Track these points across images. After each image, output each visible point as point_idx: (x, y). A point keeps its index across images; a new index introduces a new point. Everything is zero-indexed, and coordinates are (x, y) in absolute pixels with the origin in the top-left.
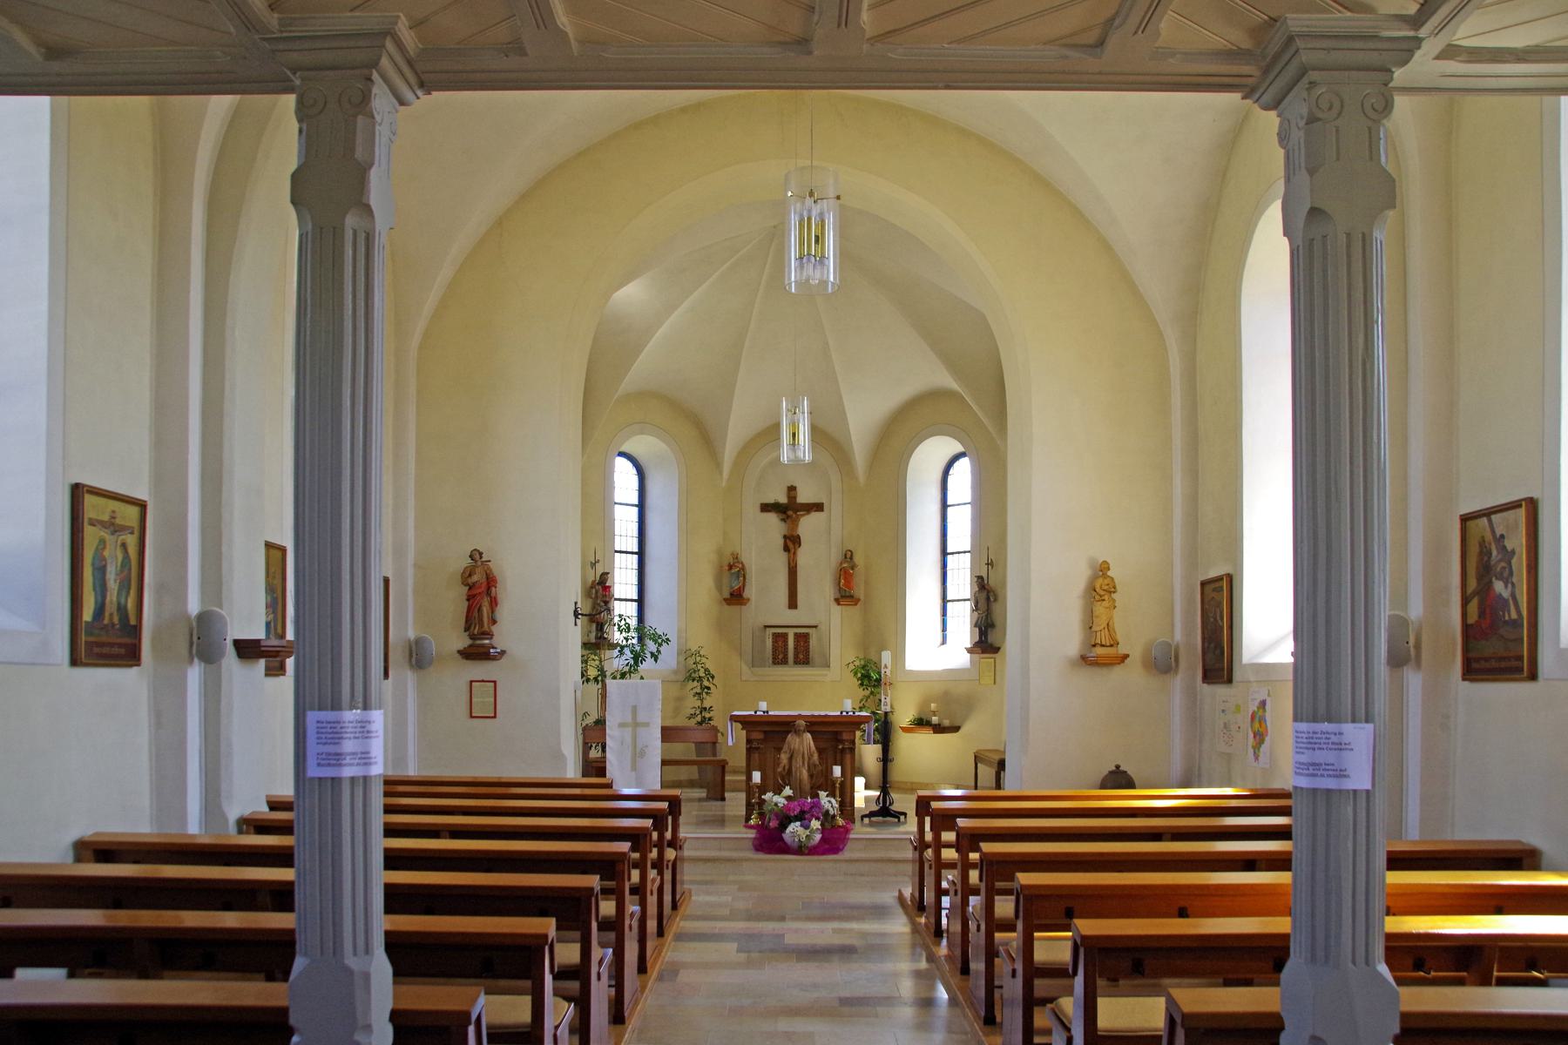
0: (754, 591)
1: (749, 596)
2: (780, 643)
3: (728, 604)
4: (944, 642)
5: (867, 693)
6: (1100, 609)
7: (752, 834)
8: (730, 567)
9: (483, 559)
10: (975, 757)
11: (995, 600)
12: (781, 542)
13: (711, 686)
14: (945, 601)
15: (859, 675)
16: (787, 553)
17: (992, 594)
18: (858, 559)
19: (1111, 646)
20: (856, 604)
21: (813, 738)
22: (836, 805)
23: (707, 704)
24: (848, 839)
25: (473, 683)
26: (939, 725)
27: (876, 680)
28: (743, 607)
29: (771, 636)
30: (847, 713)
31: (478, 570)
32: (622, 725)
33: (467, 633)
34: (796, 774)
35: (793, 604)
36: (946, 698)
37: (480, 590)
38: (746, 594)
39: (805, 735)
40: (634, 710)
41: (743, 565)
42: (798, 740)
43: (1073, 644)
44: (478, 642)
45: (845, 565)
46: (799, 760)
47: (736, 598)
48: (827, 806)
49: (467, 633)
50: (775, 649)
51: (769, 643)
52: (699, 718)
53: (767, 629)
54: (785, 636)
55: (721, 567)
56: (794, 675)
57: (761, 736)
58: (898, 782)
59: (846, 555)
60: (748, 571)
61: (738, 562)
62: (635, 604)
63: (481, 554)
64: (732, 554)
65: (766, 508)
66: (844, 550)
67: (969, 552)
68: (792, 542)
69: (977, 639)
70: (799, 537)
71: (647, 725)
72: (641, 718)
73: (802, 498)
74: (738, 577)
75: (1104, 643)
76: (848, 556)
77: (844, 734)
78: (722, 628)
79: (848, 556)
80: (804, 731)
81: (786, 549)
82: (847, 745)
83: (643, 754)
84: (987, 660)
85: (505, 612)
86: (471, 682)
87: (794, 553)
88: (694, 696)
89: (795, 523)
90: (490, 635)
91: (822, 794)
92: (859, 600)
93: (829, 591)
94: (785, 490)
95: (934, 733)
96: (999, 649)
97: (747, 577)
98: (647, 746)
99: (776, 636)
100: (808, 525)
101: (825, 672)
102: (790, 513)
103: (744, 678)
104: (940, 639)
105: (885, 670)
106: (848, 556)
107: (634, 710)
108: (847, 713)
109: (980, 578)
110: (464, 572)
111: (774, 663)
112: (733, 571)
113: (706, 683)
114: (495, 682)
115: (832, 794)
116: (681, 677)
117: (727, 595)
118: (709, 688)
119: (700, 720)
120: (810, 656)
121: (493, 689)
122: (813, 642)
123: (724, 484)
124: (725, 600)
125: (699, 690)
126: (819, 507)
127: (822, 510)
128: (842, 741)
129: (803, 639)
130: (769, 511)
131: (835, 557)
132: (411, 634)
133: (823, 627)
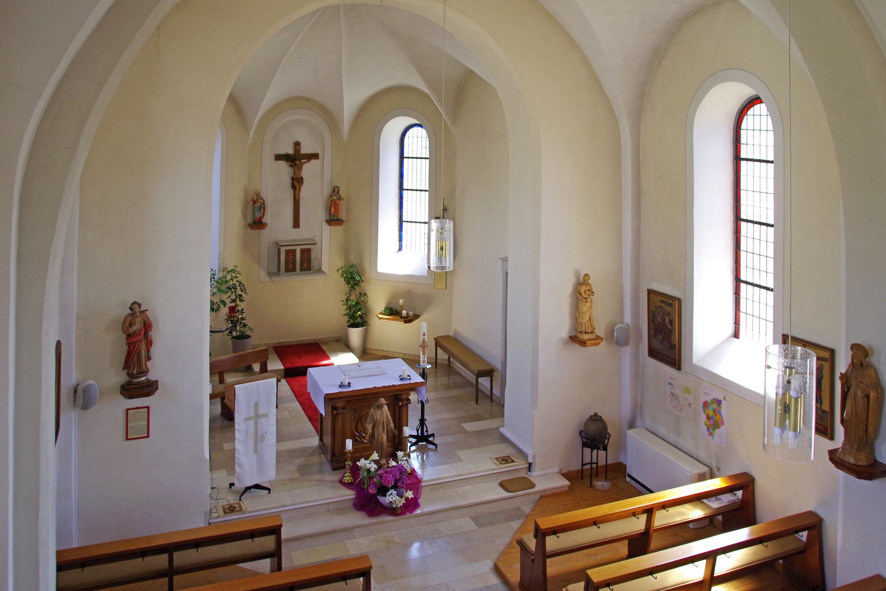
1: (266, 222)
2: (291, 257)
4: (400, 249)
7: (350, 494)
9: (141, 309)
16: (626, 556)
18: (342, 192)
25: (129, 411)
29: (284, 253)
33: (125, 371)
34: (378, 437)
35: (296, 224)
36: (409, 294)
37: (139, 338)
38: (264, 220)
41: (264, 201)
43: (565, 331)
44: (136, 380)
45: (334, 198)
47: (258, 224)
49: (125, 371)
54: (294, 251)
60: (266, 205)
61: (260, 198)
63: (140, 305)
65: (278, 157)
66: (333, 186)
68: (297, 182)
70: (302, 178)
72: (262, 411)
73: (304, 151)
75: (587, 331)
78: (246, 245)
79: (336, 190)
81: (294, 187)
83: (263, 438)
85: (156, 350)
86: (128, 410)
89: (300, 168)
93: (321, 214)
94: (293, 144)
97: (266, 208)
98: (266, 433)
99: (287, 252)
100: (308, 170)
103: (261, 280)
104: (397, 247)
105: (424, 337)
106: (335, 190)
107: (257, 405)
110: (124, 322)
112: (256, 205)
123: (249, 142)
126: (315, 156)
127: (318, 158)
129: (306, 253)
130: (282, 160)
131: (327, 191)
132: (74, 380)
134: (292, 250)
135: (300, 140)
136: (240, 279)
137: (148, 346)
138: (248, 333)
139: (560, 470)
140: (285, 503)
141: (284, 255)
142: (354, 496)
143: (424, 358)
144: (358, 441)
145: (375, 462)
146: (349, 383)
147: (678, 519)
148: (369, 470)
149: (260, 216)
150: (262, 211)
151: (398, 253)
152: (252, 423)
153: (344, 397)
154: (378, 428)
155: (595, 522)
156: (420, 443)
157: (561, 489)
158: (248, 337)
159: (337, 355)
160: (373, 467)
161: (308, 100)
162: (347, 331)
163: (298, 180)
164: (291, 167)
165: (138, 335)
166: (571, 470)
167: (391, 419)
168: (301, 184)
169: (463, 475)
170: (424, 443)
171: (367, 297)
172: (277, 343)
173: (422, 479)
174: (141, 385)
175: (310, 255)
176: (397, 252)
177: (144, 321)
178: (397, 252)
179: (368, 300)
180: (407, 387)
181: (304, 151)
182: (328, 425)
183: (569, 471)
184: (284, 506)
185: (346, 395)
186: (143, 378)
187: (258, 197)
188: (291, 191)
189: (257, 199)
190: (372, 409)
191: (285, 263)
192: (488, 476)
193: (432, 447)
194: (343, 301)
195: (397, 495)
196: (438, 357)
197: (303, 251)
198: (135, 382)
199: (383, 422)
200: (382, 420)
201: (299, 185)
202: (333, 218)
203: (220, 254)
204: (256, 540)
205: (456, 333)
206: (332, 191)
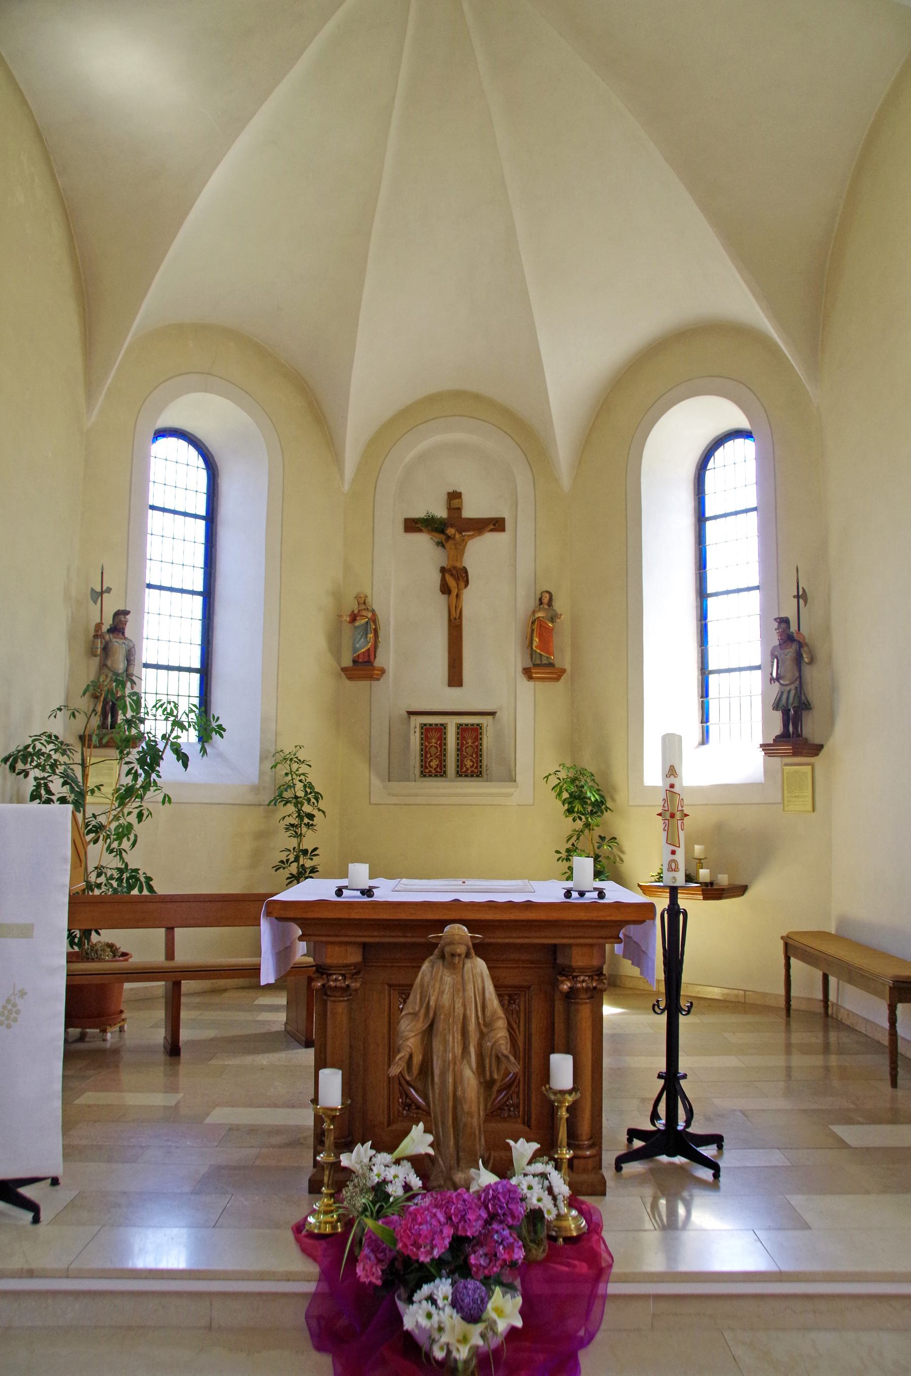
0: (392, 655)
2: (434, 741)
3: (350, 678)
5: (579, 824)
10: (786, 945)
11: (812, 661)
12: (435, 578)
13: (315, 812)
14: (704, 672)
15: (565, 795)
16: (445, 596)
17: (805, 649)
18: (559, 605)
20: (558, 679)
21: (489, 968)
22: (562, 1189)
23: (307, 844)
24: (605, 1297)
26: (712, 884)
27: (594, 804)
28: (375, 683)
29: (418, 730)
30: (582, 894)
34: (443, 1074)
35: (455, 678)
38: (378, 662)
39: (468, 964)
42: (448, 979)
48: (536, 1197)
50: (424, 753)
51: (415, 740)
52: (293, 869)
53: (413, 718)
54: (441, 729)
56: (465, 795)
57: (354, 957)
59: (540, 599)
62: (196, 677)
64: (357, 597)
65: (412, 525)
67: (757, 588)
69: (778, 729)
70: (465, 571)
73: (469, 512)
74: (366, 634)
76: (546, 600)
77: (575, 951)
79: (546, 600)
80: (468, 955)
81: (445, 589)
82: (583, 982)
84: (800, 768)
87: (457, 596)
88: (287, 829)
89: (460, 550)
91: (523, 1149)
95: (705, 898)
96: (821, 747)
97: (381, 634)
98: (23, 994)
99: (426, 730)
101: (511, 790)
102: (451, 531)
103: (373, 800)
106: (545, 601)
108: (582, 894)
109: (784, 622)
111: (423, 774)
112: (357, 624)
113: (307, 808)
115: (547, 1150)
116: (267, 797)
117: (347, 662)
118: (311, 816)
119: (295, 872)
120: (485, 763)
122: (488, 741)
123: (346, 487)
124: (344, 670)
125: (295, 821)
126: (498, 525)
127: (503, 530)
128: (567, 971)
130: (420, 531)
131: (524, 603)
133: (503, 715)
141: (418, 734)
142: (310, 1287)
143: (673, 852)
144: (418, 1107)
145: (419, 1163)
148: (380, 1190)
149: (366, 648)
150: (371, 636)
151: (698, 749)
154: (445, 1042)
156: (664, 1158)
160: (406, 1174)
161: (477, 397)
163: (454, 572)
164: (440, 549)
167: (500, 1013)
168: (462, 584)
169: (81, 1274)
170: (679, 1160)
171: (622, 852)
173: (610, 1266)
176: (697, 747)
178: (697, 747)
181: (469, 512)
182: (406, 1087)
184: (31, 1274)
187: (363, 607)
188: (441, 601)
189: (359, 611)
190: (426, 966)
193: (706, 1174)
194: (558, 852)
195: (454, 1304)
196: (792, 994)
197: (462, 730)
199: (465, 1018)
202: (538, 662)
203: (265, 720)
205: (843, 922)
206: (538, 602)
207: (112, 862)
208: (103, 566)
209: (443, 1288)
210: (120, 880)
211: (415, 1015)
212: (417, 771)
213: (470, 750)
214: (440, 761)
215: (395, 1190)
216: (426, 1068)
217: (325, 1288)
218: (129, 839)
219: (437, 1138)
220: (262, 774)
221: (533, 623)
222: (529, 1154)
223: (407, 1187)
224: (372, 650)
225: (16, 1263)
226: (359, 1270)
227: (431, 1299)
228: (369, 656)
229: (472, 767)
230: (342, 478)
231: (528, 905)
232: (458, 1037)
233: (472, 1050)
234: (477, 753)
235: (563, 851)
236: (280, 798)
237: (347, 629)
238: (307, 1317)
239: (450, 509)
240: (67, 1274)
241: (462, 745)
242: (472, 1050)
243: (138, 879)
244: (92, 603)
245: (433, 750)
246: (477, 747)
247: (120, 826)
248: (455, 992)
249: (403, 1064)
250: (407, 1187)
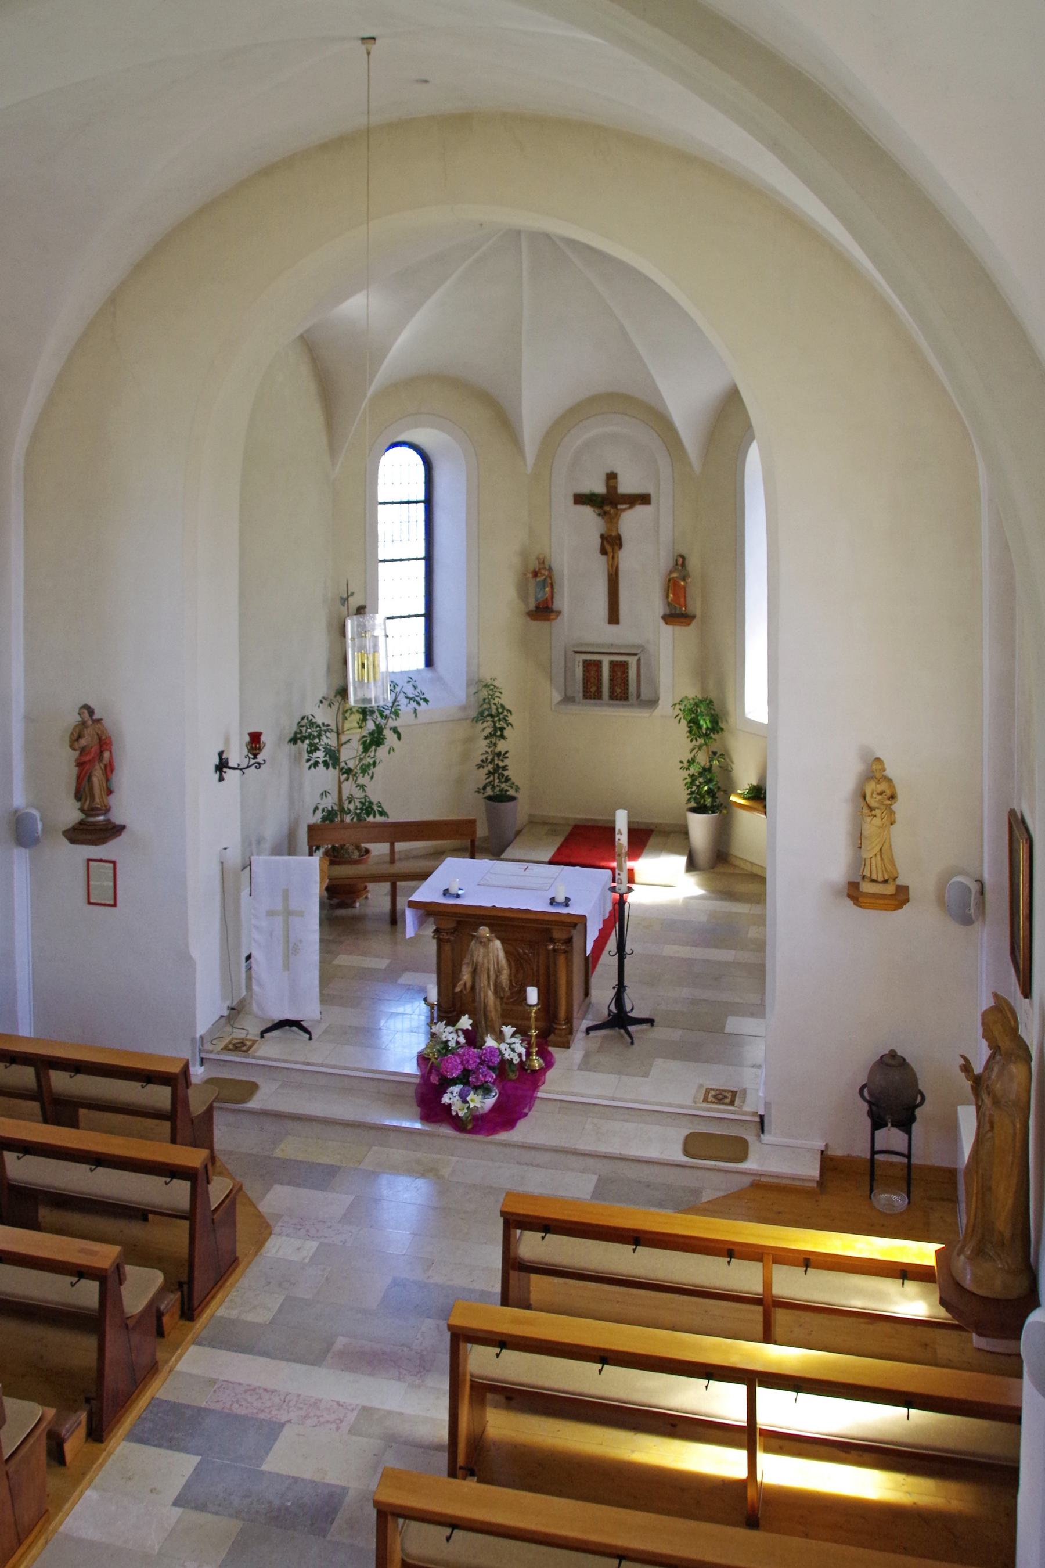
0: (566, 600)
2: (592, 672)
6: (872, 826)
8: (535, 574)
12: (597, 542)
18: (694, 564)
19: (886, 881)
24: (536, 1098)
29: (581, 664)
31: (87, 732)
32: (271, 913)
34: (480, 991)
35: (614, 617)
38: (556, 605)
39: (491, 944)
40: (286, 895)
42: (482, 950)
44: (92, 819)
45: (674, 575)
46: (484, 977)
50: (586, 681)
52: (490, 767)
53: (577, 655)
54: (598, 664)
55: (525, 574)
58: (736, 857)
61: (545, 568)
64: (538, 558)
65: (580, 499)
66: (676, 554)
68: (611, 543)
71: (301, 914)
73: (625, 487)
75: (874, 877)
76: (680, 560)
81: (603, 551)
83: (296, 951)
86: (89, 860)
87: (613, 557)
90: (107, 810)
92: (694, 617)
93: (658, 607)
94: (604, 477)
97: (555, 587)
107: (286, 895)
111: (585, 697)
112: (538, 579)
114: (114, 863)
116: (474, 713)
117: (532, 606)
121: (112, 871)
126: (644, 499)
129: (619, 669)
131: (664, 562)
134: (594, 661)
135: (617, 470)
136: (502, 701)
137: (106, 773)
138: (511, 792)
139: (826, 1146)
140: (312, 1060)
141: (581, 668)
142: (417, 1081)
145: (465, 1032)
146: (567, 899)
147: (858, 1303)
150: (548, 589)
152: (279, 920)
153: (455, 914)
155: (730, 1251)
157: (797, 1183)
158: (512, 799)
159: (659, 855)
162: (685, 819)
165: (87, 754)
166: (854, 1154)
168: (616, 548)
169: (327, 1066)
172: (582, 819)
174: (93, 828)
175: (627, 672)
177: (98, 735)
179: (733, 766)
180: (553, 918)
183: (849, 1156)
184: (308, 1064)
185: (538, 917)
186: (101, 818)
187: (542, 566)
189: (539, 569)
191: (584, 683)
192: (691, 1118)
194: (681, 762)
197: (613, 664)
198: (88, 822)
199: (488, 969)
200: (486, 965)
201: (613, 549)
204: (14, 1067)
207: (359, 794)
208: (417, 81)
209: (456, 1089)
210: (361, 809)
211: (468, 964)
212: (581, 695)
213: (619, 680)
214: (598, 687)
215: (452, 1044)
216: (473, 988)
217: (422, 1082)
218: (369, 774)
219: (474, 1021)
220: (468, 696)
221: (669, 581)
222: (511, 1034)
223: (458, 1043)
224: (549, 599)
225: (302, 1059)
226: (431, 1078)
227: (452, 1093)
228: (547, 603)
229: (621, 693)
230: (525, 464)
231: (527, 911)
232: (486, 976)
233: (492, 983)
234: (624, 683)
235: (685, 761)
236: (481, 717)
237: (532, 583)
238: (415, 1093)
239: (608, 486)
240: (322, 1066)
241: (614, 676)
242: (492, 983)
243: (372, 809)
244: (342, 607)
245: (592, 680)
246: (624, 678)
247: (363, 764)
248: (484, 957)
249: (462, 986)
250: (458, 1043)
